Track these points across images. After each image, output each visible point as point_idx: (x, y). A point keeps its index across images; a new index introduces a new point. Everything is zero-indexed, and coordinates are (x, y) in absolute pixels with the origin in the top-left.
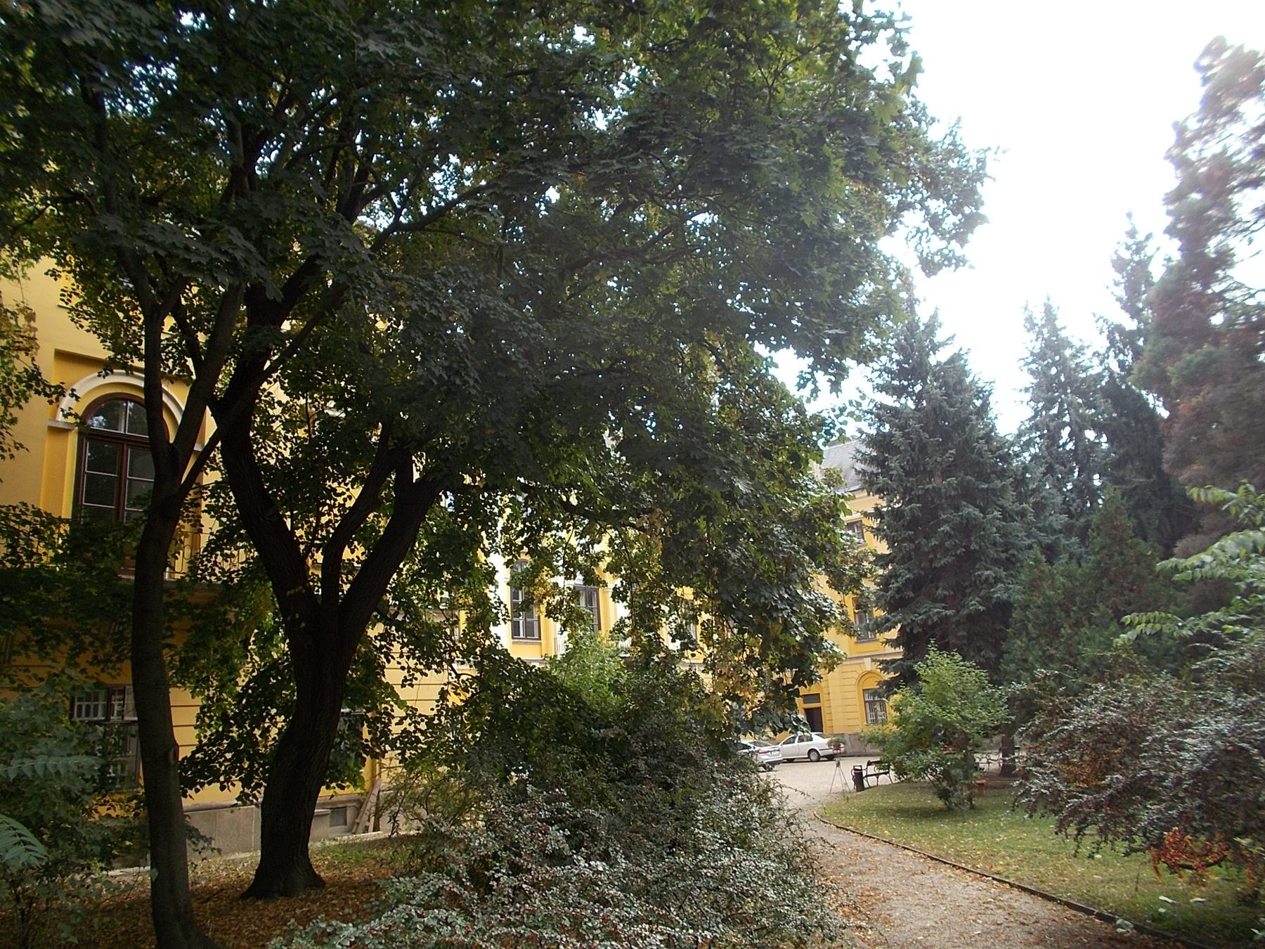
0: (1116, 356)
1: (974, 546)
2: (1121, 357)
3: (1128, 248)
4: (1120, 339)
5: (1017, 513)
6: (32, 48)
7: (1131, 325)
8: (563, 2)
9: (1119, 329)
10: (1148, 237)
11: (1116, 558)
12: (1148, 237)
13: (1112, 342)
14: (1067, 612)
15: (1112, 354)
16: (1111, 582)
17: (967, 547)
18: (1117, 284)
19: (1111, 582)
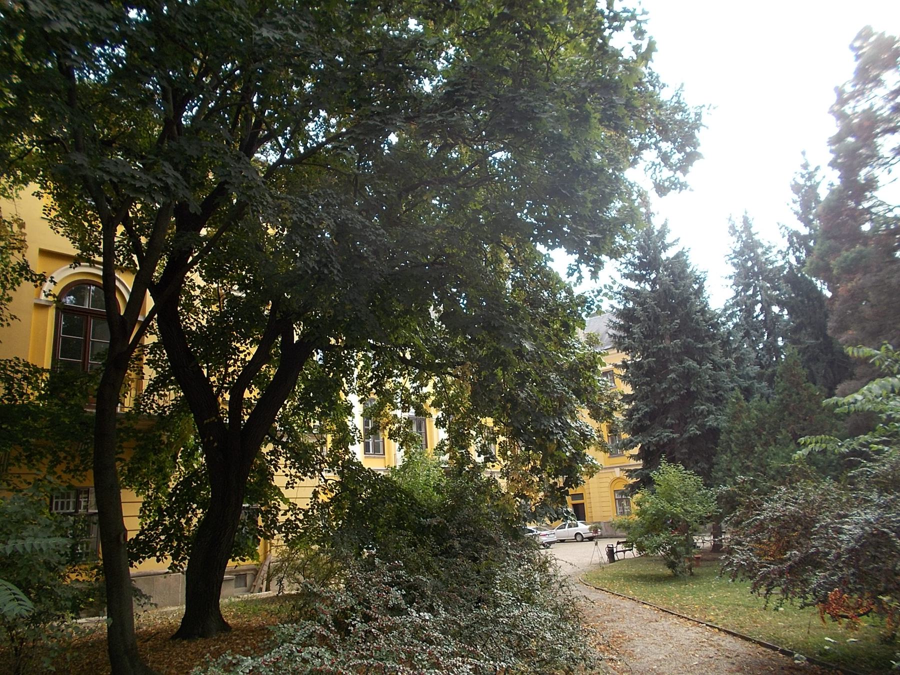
0: (794, 253)
1: (693, 389)
2: (798, 254)
3: (803, 176)
4: (797, 241)
5: (724, 365)
6: (23, 34)
7: (805, 231)
8: (400, 2)
9: (796, 234)
10: (817, 169)
11: (794, 397)
12: (817, 169)
13: (791, 243)
14: (759, 435)
15: (791, 252)
16: (790, 414)
17: (688, 389)
18: (795, 202)
19: (790, 414)
